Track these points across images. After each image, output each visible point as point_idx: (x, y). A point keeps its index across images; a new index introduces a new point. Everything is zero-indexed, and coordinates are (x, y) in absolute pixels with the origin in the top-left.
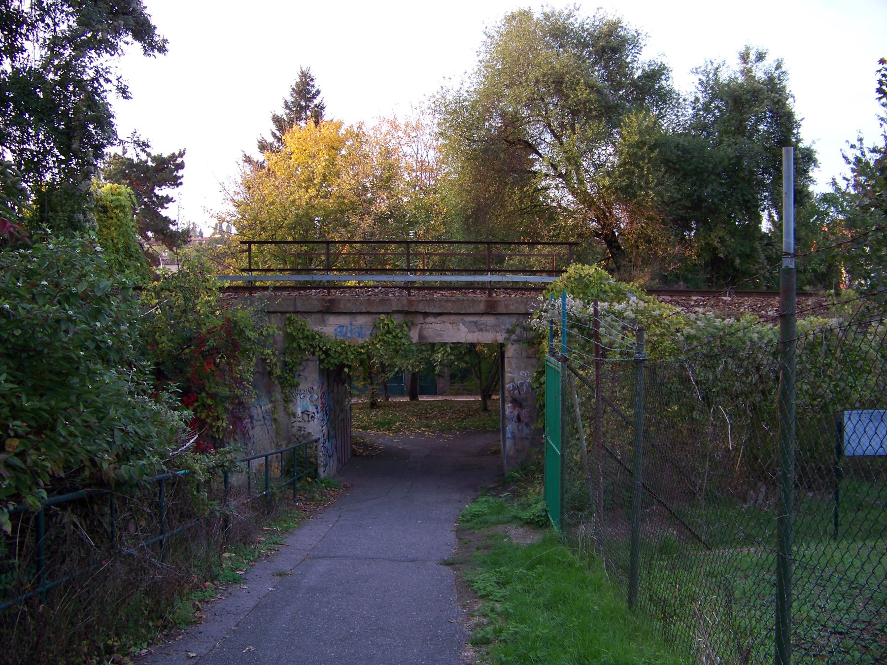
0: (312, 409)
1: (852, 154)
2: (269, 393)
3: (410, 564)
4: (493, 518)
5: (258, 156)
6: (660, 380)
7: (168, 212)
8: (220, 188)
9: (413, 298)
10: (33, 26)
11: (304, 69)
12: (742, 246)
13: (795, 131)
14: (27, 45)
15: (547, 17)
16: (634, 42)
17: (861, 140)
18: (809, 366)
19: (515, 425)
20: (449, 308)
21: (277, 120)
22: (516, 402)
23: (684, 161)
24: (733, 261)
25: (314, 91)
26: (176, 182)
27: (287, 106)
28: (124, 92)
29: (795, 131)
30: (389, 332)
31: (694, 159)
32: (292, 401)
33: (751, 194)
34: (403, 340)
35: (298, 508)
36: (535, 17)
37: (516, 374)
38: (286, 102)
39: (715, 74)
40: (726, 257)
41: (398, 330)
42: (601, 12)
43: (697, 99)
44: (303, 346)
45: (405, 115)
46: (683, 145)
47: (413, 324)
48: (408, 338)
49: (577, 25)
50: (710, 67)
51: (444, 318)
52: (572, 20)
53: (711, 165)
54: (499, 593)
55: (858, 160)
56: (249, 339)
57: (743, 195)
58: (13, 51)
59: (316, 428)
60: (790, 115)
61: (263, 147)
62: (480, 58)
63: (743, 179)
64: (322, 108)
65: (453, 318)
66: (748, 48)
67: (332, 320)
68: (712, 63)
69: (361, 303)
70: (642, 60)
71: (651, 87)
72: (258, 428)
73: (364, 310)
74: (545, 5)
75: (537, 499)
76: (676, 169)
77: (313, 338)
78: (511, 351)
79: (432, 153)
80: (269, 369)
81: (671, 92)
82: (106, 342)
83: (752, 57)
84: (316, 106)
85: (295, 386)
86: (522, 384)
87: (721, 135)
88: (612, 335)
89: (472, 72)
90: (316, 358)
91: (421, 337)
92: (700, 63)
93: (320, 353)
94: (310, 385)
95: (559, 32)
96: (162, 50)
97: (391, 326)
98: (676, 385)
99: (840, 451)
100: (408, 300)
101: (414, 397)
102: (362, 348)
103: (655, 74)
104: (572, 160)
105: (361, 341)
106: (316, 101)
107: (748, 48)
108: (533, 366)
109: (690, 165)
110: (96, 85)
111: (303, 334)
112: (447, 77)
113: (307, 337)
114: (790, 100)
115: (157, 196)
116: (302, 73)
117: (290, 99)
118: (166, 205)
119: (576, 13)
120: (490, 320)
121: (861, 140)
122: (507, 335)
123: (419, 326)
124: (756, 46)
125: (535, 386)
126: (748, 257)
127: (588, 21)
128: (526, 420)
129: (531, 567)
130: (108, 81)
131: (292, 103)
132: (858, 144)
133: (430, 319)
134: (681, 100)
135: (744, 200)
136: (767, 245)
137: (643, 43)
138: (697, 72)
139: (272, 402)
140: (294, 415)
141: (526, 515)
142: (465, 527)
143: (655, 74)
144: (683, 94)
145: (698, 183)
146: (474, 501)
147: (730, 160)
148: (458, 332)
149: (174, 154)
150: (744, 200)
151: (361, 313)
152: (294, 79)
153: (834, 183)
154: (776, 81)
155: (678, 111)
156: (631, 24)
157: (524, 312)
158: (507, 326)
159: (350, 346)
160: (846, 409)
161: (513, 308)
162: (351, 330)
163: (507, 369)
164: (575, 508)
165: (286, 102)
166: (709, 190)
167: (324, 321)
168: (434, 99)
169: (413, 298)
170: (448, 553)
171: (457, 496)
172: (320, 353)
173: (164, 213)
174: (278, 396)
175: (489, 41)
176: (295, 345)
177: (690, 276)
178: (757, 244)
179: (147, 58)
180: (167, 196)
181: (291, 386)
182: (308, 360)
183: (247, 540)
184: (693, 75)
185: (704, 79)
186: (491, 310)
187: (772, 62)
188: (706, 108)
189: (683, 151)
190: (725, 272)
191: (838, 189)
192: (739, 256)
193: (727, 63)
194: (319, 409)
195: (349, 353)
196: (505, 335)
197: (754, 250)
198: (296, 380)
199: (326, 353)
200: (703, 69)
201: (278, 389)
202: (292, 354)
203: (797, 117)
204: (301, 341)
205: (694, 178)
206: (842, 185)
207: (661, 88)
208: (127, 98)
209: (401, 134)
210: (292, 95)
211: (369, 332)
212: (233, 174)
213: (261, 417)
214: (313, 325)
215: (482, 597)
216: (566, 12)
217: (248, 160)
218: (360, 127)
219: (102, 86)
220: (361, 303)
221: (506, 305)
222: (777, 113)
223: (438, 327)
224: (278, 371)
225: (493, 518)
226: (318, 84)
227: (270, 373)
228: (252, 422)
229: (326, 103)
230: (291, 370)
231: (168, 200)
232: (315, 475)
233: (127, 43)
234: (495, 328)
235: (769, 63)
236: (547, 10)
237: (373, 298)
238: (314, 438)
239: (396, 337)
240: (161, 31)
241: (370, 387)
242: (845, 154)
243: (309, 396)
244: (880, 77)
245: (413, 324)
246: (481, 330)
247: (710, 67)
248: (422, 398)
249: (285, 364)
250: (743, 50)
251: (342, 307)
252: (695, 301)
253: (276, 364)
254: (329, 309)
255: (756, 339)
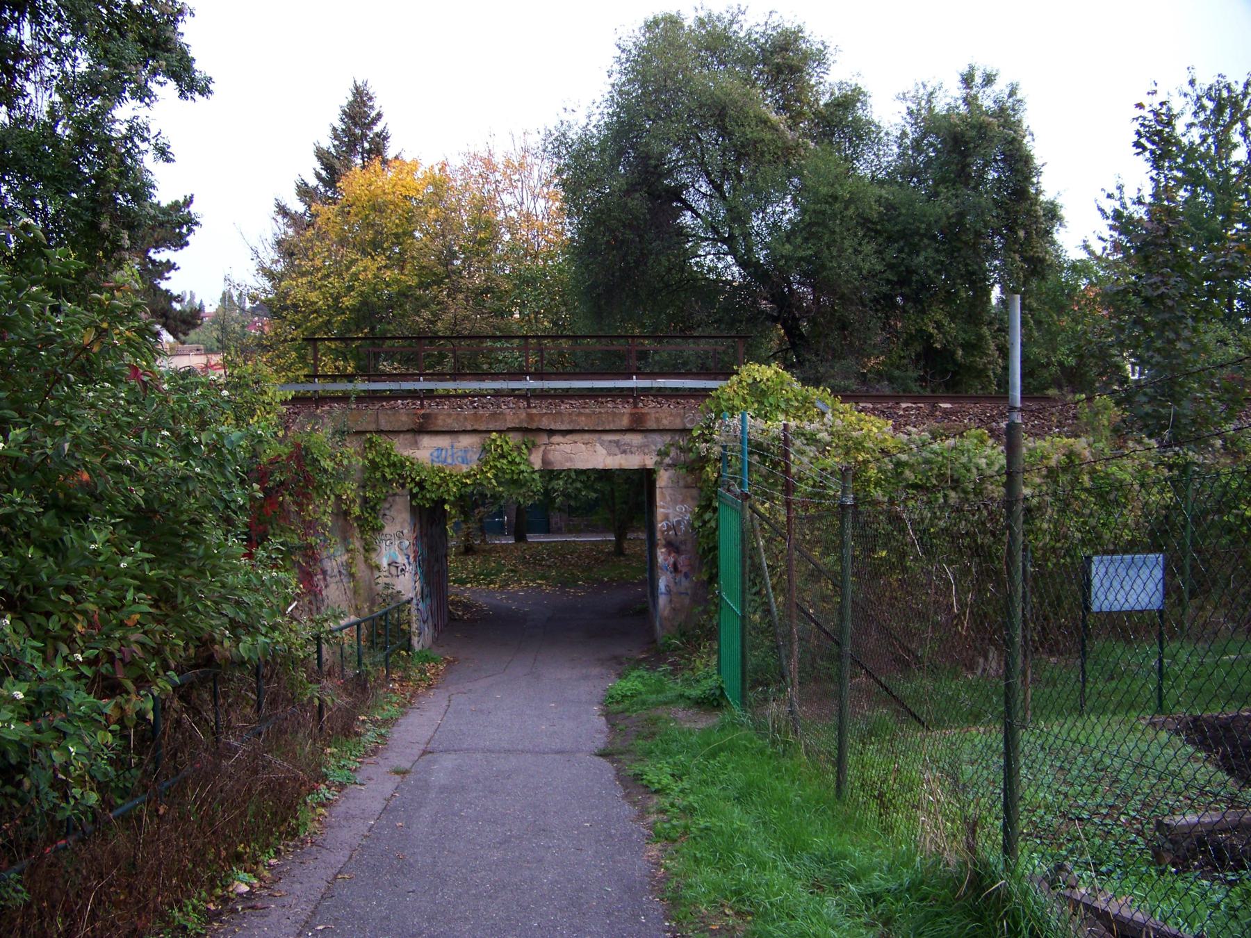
0: (401, 560)
1: (1110, 206)
2: (345, 540)
3: (558, 757)
4: (653, 698)
5: (298, 207)
6: (855, 515)
7: (173, 284)
8: (250, 254)
9: (534, 411)
10: (37, 60)
11: (359, 83)
12: (965, 332)
13: (1035, 180)
14: (30, 88)
15: (701, 23)
16: (819, 57)
17: (1120, 188)
18: (1048, 498)
19: (670, 575)
20: (583, 423)
21: (321, 155)
22: (672, 546)
23: (888, 221)
24: (953, 353)
25: (373, 114)
26: (180, 243)
27: (336, 137)
28: (163, 153)
29: (1035, 180)
30: (502, 456)
31: (902, 218)
32: (375, 550)
33: (977, 263)
34: (522, 467)
35: (393, 690)
36: (686, 24)
37: (671, 509)
38: (334, 129)
39: (929, 101)
40: (944, 347)
41: (515, 454)
42: (775, 17)
43: (904, 134)
44: (389, 477)
45: (503, 150)
46: (887, 199)
47: (534, 445)
48: (529, 464)
49: (742, 34)
50: (921, 91)
51: (576, 437)
52: (735, 27)
53: (923, 226)
54: (676, 787)
55: (1117, 215)
56: (325, 471)
57: (966, 265)
58: (8, 97)
59: (407, 584)
60: (1027, 159)
61: (304, 192)
62: (612, 81)
63: (966, 243)
64: (385, 138)
65: (587, 437)
66: (972, 68)
67: (426, 441)
68: (925, 86)
69: (465, 418)
70: (831, 80)
71: (842, 120)
72: (333, 587)
73: (469, 428)
74: (699, 7)
75: (708, 672)
76: (877, 232)
77: (403, 466)
78: (663, 479)
79: (541, 203)
80: (344, 507)
81: (870, 123)
82: (235, 501)
83: (978, 80)
84: (378, 135)
85: (378, 530)
86: (679, 522)
87: (936, 184)
88: (803, 461)
89: (601, 99)
90: (406, 492)
91: (545, 461)
92: (909, 87)
93: (412, 485)
94: (398, 528)
95: (716, 41)
96: (205, 91)
97: (506, 448)
98: (883, 526)
99: (1088, 608)
100: (528, 414)
101: (520, 538)
102: (466, 477)
103: (848, 101)
104: (738, 217)
105: (465, 469)
106: (377, 129)
107: (972, 68)
108: (693, 498)
109: (896, 224)
110: (130, 145)
111: (388, 460)
112: (569, 109)
113: (394, 465)
114: (1028, 138)
115: (153, 262)
116: (357, 89)
117: (340, 126)
118: (167, 275)
119: (741, 17)
120: (636, 439)
121: (1120, 188)
122: (658, 458)
123: (543, 448)
124: (984, 64)
125: (697, 524)
126: (974, 347)
127: (757, 29)
128: (684, 570)
129: (714, 755)
130: (144, 140)
131: (343, 130)
132: (1117, 193)
133: (557, 439)
134: (882, 134)
135: (967, 271)
136: (999, 330)
137: (832, 59)
138: (904, 98)
139: (348, 551)
140: (378, 568)
141: (695, 692)
142: (614, 711)
143: (848, 101)
144: (885, 125)
145: (906, 250)
146: (620, 676)
147: (949, 218)
148: (594, 455)
149: (177, 202)
150: (967, 271)
151: (465, 432)
152: (345, 97)
153: (1086, 247)
154: (1010, 112)
155: (879, 150)
156: (815, 33)
157: (680, 427)
158: (659, 446)
159: (451, 475)
160: (1096, 553)
161: (666, 423)
162: (452, 455)
163: (659, 502)
164: (759, 680)
165: (334, 129)
166: (921, 259)
167: (416, 442)
168: (552, 139)
169: (534, 411)
170: (600, 741)
171: (595, 671)
172: (412, 485)
173: (164, 285)
174: (357, 544)
175: (624, 56)
176: (378, 475)
177: (897, 373)
178: (985, 330)
179: (184, 102)
180: (168, 261)
181: (373, 529)
182: (395, 495)
183: (348, 731)
184: (898, 102)
185: (914, 107)
186: (637, 426)
187: (1004, 87)
188: (917, 145)
189: (886, 208)
190: (946, 375)
191: (1091, 253)
192: (962, 346)
193: (945, 87)
194: (411, 560)
195: (451, 485)
196: (655, 458)
197: (981, 337)
198: (380, 521)
199: (420, 484)
200: (912, 94)
201: (357, 534)
202: (374, 487)
203: (1037, 162)
204: (387, 470)
205: (902, 243)
206: (1097, 247)
207: (857, 120)
208: (168, 160)
209: (498, 176)
210: (342, 120)
211: (476, 457)
212: (267, 230)
213: (336, 571)
214: (401, 449)
215: (657, 792)
216: (728, 17)
217: (283, 211)
218: (442, 169)
219: (137, 147)
220: (465, 418)
221: (657, 419)
222: (1011, 156)
223: (568, 448)
224: (356, 510)
225: (653, 698)
226: (379, 104)
227: (346, 513)
228: (325, 579)
229: (391, 131)
230: (373, 508)
231: (170, 266)
232: (409, 647)
233: (161, 84)
234: (642, 448)
235: (1000, 88)
236: (702, 14)
237: (481, 412)
238: (405, 598)
239: (512, 462)
240: (202, 66)
241: (464, 526)
242: (1102, 206)
243: (397, 542)
244: (1138, 127)
245: (534, 445)
246: (624, 452)
247: (921, 91)
248: (532, 538)
249: (365, 500)
250: (965, 70)
251: (440, 424)
252: (905, 410)
253: (354, 501)
254: (423, 428)
255: (984, 466)
